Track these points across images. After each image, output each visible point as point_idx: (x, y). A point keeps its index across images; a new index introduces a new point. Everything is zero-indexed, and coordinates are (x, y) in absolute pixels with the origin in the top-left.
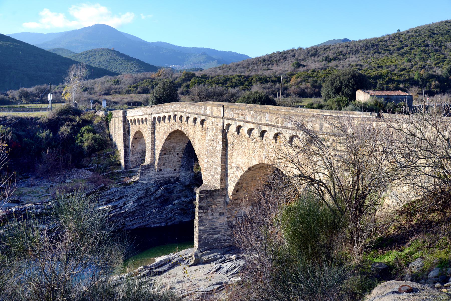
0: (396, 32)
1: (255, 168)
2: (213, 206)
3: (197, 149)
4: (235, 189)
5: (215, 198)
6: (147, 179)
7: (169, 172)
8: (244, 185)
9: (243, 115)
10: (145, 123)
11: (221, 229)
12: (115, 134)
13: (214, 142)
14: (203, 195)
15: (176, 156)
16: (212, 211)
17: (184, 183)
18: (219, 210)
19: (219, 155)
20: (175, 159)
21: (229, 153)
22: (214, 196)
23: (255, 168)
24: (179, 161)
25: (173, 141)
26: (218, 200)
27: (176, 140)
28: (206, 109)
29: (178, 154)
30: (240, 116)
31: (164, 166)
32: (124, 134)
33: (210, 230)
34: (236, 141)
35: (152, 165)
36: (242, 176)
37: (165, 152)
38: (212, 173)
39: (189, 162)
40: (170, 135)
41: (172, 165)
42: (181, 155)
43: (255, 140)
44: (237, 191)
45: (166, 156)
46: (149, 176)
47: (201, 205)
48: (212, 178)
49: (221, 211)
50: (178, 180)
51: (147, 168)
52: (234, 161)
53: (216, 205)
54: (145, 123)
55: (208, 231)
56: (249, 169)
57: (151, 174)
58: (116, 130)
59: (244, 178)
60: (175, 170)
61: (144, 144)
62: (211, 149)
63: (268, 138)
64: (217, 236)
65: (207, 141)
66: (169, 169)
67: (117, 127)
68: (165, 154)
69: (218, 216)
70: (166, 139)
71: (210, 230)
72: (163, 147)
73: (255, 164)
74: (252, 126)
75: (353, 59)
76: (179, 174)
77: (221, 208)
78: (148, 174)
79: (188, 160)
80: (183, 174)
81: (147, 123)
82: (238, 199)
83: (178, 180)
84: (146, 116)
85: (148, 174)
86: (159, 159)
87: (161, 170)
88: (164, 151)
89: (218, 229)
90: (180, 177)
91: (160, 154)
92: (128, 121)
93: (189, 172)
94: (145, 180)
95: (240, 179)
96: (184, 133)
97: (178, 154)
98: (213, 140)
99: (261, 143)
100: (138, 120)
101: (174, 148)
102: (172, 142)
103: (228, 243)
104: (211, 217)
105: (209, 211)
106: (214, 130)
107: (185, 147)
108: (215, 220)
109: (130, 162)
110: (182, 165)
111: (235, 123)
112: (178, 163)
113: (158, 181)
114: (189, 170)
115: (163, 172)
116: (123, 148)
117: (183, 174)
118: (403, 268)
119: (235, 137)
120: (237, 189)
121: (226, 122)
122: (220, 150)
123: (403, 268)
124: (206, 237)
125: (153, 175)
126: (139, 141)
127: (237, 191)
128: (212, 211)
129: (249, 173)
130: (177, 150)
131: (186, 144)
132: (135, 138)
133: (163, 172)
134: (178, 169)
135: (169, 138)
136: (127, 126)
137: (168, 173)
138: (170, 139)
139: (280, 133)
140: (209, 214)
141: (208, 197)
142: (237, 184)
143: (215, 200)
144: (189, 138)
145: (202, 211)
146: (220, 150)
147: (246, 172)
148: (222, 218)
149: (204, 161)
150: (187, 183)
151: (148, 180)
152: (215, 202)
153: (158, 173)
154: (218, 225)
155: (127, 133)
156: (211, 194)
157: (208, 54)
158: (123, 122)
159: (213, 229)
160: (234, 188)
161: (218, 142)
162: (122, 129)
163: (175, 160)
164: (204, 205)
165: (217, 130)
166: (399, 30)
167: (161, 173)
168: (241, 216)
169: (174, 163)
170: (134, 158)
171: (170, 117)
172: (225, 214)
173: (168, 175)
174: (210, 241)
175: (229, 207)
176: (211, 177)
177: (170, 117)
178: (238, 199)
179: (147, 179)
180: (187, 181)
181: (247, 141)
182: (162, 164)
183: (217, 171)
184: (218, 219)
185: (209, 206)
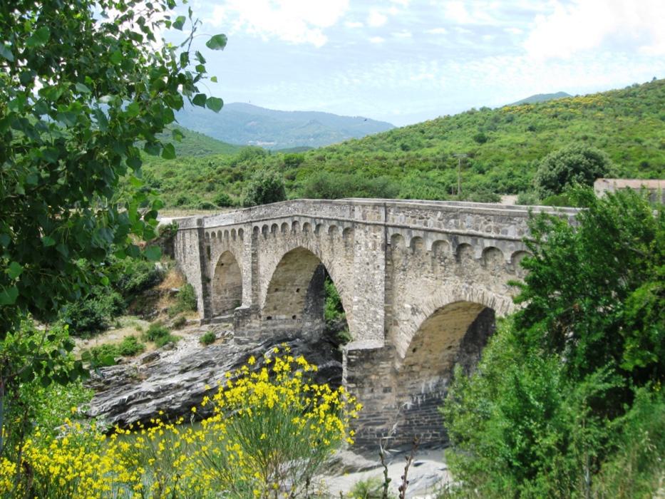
0: (650, 80)
1: (446, 310)
2: (373, 377)
3: (338, 279)
4: (410, 347)
5: (375, 362)
6: (246, 333)
7: (284, 322)
8: (426, 340)
9: (423, 218)
10: (238, 238)
11: (387, 417)
12: (184, 257)
13: (370, 265)
14: (354, 357)
15: (296, 293)
16: (371, 384)
17: (309, 340)
18: (383, 384)
19: (380, 287)
20: (294, 299)
21: (398, 285)
22: (373, 359)
23: (446, 310)
24: (301, 302)
25: (291, 268)
26: (381, 366)
27: (295, 266)
28: (353, 210)
29: (298, 290)
30: (417, 220)
31: (275, 312)
32: (202, 258)
33: (368, 417)
34: (410, 264)
35: (255, 309)
36: (423, 324)
37: (277, 287)
38: (368, 320)
39: (317, 304)
40: (286, 257)
41: (288, 309)
42: (304, 292)
43: (446, 261)
44: (414, 350)
45: (279, 293)
46: (249, 328)
47: (352, 374)
48: (368, 329)
49: (387, 386)
50: (299, 335)
51: (246, 313)
52: (408, 298)
53: (377, 374)
54: (238, 238)
55: (364, 418)
56: (436, 311)
57: (253, 325)
58: (188, 251)
59: (426, 329)
60: (294, 317)
61: (238, 273)
62: (365, 279)
63: (470, 258)
64: (380, 427)
65: (358, 266)
66: (284, 317)
67: (188, 246)
68: (277, 290)
69: (381, 394)
70: (279, 264)
71: (368, 417)
72: (273, 279)
73: (448, 302)
74: (440, 237)
75: (578, 126)
76: (301, 325)
77: (388, 380)
78: (248, 325)
79: (315, 300)
80: (308, 324)
81: (242, 239)
82: (415, 364)
83: (299, 335)
84: (242, 226)
85: (248, 325)
86: (267, 300)
87: (269, 318)
88: (275, 287)
89: (382, 416)
90: (303, 330)
91: (269, 289)
92: (207, 234)
93: (318, 321)
94: (243, 335)
95: (420, 330)
96: (313, 254)
97: (298, 290)
98: (368, 264)
99: (458, 266)
100: (226, 232)
101: (293, 280)
102: (288, 270)
103: (400, 439)
104: (369, 396)
105: (367, 385)
106: (370, 245)
107: (311, 277)
108: (377, 401)
109: (213, 305)
110: (306, 310)
111: (409, 233)
112: (299, 306)
113: (267, 337)
114: (317, 317)
115: (274, 322)
116: (200, 281)
117: (308, 324)
118: (479, 439)
119: (409, 257)
120: (414, 347)
121: (391, 232)
122: (381, 280)
123: (479, 439)
124: (363, 430)
125: (258, 326)
126: (228, 269)
127: (414, 350)
128: (371, 384)
129: (435, 319)
130: (296, 283)
131: (313, 273)
132: (220, 264)
133: (274, 322)
134: (298, 316)
135: (284, 262)
136: (206, 244)
137: (281, 323)
138: (285, 264)
139: (499, 250)
140: (366, 390)
141: (362, 360)
142: (415, 339)
143: (376, 367)
144: (323, 262)
145: (354, 385)
146: (381, 280)
147: (432, 316)
148: (388, 395)
149: (351, 300)
150: (314, 341)
151: (249, 334)
152: (375, 370)
153: (266, 322)
154: (381, 408)
155: (206, 255)
156: (367, 356)
157: (315, 118)
158: (200, 237)
159: (374, 416)
160: (408, 345)
161: (378, 267)
162: (197, 248)
163: (294, 300)
164: (358, 374)
165: (375, 245)
166: (655, 78)
167: (269, 322)
168: (420, 394)
169: (292, 306)
170: (219, 297)
171: (284, 225)
172: (393, 390)
173: (282, 326)
174: (369, 437)
175: (401, 378)
176: (366, 327)
177: (275, 226)
178: (415, 364)
179: (246, 333)
180: (315, 336)
181: (430, 263)
182: (271, 308)
183: (378, 317)
184: (382, 398)
185: (366, 377)
